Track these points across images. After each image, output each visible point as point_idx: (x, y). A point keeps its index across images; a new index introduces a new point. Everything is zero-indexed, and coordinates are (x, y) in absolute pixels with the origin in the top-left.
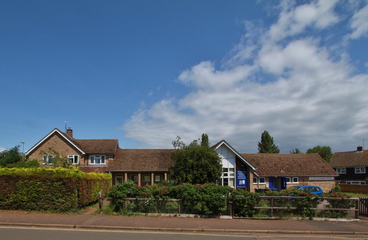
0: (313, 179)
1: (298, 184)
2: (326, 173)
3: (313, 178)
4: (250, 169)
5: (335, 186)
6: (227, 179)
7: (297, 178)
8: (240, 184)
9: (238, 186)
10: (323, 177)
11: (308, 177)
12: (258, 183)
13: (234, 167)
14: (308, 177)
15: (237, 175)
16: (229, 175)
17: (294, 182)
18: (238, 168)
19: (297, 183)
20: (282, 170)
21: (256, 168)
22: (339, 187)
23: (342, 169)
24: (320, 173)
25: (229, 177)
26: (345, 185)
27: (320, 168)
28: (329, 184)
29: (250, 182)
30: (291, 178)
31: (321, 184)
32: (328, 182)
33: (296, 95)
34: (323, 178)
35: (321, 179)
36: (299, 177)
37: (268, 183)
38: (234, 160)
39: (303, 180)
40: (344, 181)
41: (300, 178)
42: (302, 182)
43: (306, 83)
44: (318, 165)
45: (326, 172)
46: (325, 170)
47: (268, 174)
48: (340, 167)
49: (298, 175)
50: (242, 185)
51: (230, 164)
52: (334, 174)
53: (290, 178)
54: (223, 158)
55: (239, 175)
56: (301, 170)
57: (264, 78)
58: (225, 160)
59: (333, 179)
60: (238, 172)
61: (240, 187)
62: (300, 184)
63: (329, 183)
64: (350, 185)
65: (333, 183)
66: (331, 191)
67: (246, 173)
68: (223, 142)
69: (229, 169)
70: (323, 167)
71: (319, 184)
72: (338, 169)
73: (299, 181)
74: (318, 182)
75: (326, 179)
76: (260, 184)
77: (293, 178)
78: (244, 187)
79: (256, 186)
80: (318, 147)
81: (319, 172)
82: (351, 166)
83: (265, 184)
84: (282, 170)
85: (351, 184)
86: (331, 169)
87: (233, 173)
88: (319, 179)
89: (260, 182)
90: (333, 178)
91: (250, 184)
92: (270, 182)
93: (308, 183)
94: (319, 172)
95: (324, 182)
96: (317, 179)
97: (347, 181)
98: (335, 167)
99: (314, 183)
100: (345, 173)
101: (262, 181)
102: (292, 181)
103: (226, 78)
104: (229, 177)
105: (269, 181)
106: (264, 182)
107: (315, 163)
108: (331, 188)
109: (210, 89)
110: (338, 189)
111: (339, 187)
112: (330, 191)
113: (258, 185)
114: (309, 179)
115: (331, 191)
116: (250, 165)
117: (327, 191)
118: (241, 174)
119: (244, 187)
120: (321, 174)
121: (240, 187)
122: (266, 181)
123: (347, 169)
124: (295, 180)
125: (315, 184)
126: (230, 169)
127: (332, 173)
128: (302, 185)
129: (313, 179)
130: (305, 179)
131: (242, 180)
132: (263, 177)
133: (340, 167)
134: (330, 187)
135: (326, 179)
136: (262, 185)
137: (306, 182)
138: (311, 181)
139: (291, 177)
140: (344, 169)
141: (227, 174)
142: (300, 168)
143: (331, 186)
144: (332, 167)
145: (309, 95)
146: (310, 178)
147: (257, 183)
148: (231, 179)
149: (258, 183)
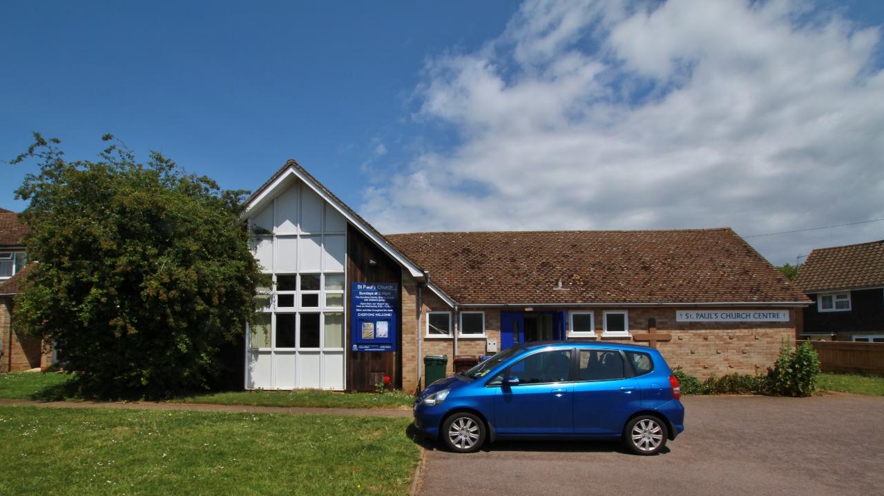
0: (693, 316)
1: (628, 338)
2: (755, 293)
3: (693, 313)
4: (404, 277)
5: (793, 349)
6: (317, 315)
7: (622, 316)
8: (364, 336)
9: (358, 345)
10: (741, 312)
11: (673, 309)
12: (454, 334)
13: (343, 271)
14: (673, 309)
15: (353, 302)
16: (322, 300)
17: (609, 329)
18: (359, 273)
19: (625, 334)
20: (560, 284)
21: (422, 272)
22: (814, 355)
23: (838, 297)
24: (725, 293)
25: (322, 308)
26: (845, 345)
27: (729, 275)
28: (769, 339)
29: (404, 327)
30: (595, 315)
31: (731, 338)
32: (761, 331)
33: (720, 129)
34: (738, 316)
35: (729, 320)
36: (630, 309)
37: (498, 334)
38: (342, 242)
39: (651, 324)
40: (845, 334)
41: (634, 315)
42: (644, 332)
43: (739, 97)
44: (723, 266)
45: (754, 290)
46: (752, 283)
47: (493, 298)
48: (828, 289)
49: (625, 301)
50: (377, 341)
51: (328, 257)
52: (787, 297)
53: (592, 314)
54: (302, 236)
55: (362, 301)
56: (645, 284)
57: (634, 91)
58: (309, 241)
59: (784, 317)
60: (359, 287)
61: (367, 348)
62: (635, 341)
63: (766, 335)
64: (868, 346)
65: (789, 335)
66: (773, 368)
67: (392, 292)
68: (291, 170)
69: (323, 278)
70: (746, 272)
71: (721, 338)
72: (824, 299)
73: (631, 328)
74: (716, 331)
75: (751, 319)
76: (460, 340)
77: (605, 313)
78: (383, 348)
79: (445, 344)
80: (787, 266)
81: (722, 291)
82: (874, 285)
83: (484, 339)
84: (560, 284)
85: (871, 341)
86: (780, 280)
87: (342, 292)
88: (720, 320)
89: (464, 332)
90: (787, 312)
91: (404, 336)
92: (504, 329)
93: (671, 336)
94: (722, 291)
95: (745, 332)
96: (714, 320)
97: (855, 334)
98: (811, 291)
99: (699, 335)
100: (850, 309)
101: (472, 325)
102: (599, 328)
103: (535, 97)
104: (322, 308)
105: (499, 324)
106: (481, 332)
107: (711, 260)
108: (777, 358)
109: (506, 127)
110: (809, 360)
111: (814, 355)
112: (769, 369)
113: (452, 340)
114: (675, 318)
115: (773, 368)
116: (390, 252)
117: (757, 367)
118: (371, 295)
119: (383, 348)
120: (730, 297)
121: (367, 348)
122: (487, 328)
123: (855, 295)
124: (615, 324)
125: (706, 339)
126: (328, 275)
127: (781, 295)
128: (646, 344)
129: (693, 316)
130: (658, 320)
131: (374, 320)
132: (478, 308)
133: (828, 289)
134: (772, 354)
135: (753, 317)
136: (473, 343)
137: (664, 332)
138: (683, 327)
139: (598, 310)
140: (845, 297)
141: (316, 296)
142: (643, 274)
143: (776, 348)
144: (804, 292)
145: (751, 130)
146: (678, 313)
147: (450, 336)
148: (332, 318)
149: (454, 334)
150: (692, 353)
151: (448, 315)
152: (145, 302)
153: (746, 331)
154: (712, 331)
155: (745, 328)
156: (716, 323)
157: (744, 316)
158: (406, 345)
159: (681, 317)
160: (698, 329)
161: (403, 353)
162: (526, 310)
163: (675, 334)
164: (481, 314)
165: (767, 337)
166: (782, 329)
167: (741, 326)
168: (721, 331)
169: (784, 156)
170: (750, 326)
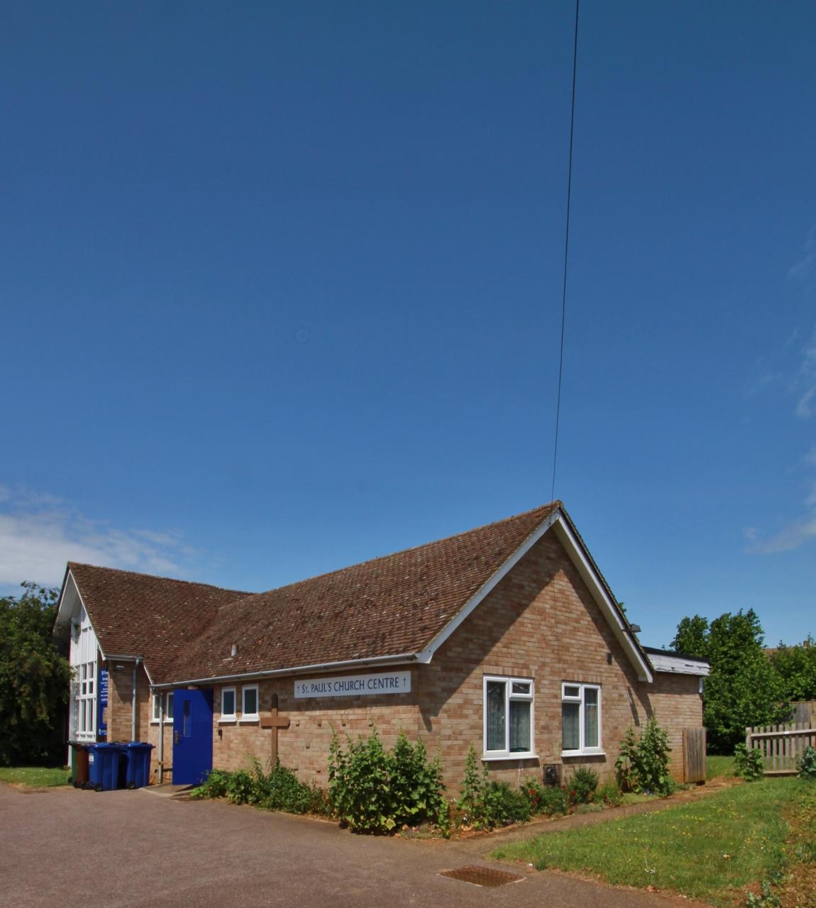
34: (352, 685)
74: (330, 712)
75: (364, 691)
138: (309, 704)
150: (308, 748)
151: (246, 691)
152: (415, 667)
153: (359, 711)
154: (325, 712)
155: (359, 707)
156: (332, 699)
157: (357, 685)
158: (282, 747)
159: (302, 690)
160: (314, 709)
161: (214, 750)
162: (190, 688)
163: (294, 717)
164: (225, 693)
165: (383, 723)
166: (401, 708)
167: (355, 703)
168: (334, 712)
169: (78, 571)
170: (363, 702)
